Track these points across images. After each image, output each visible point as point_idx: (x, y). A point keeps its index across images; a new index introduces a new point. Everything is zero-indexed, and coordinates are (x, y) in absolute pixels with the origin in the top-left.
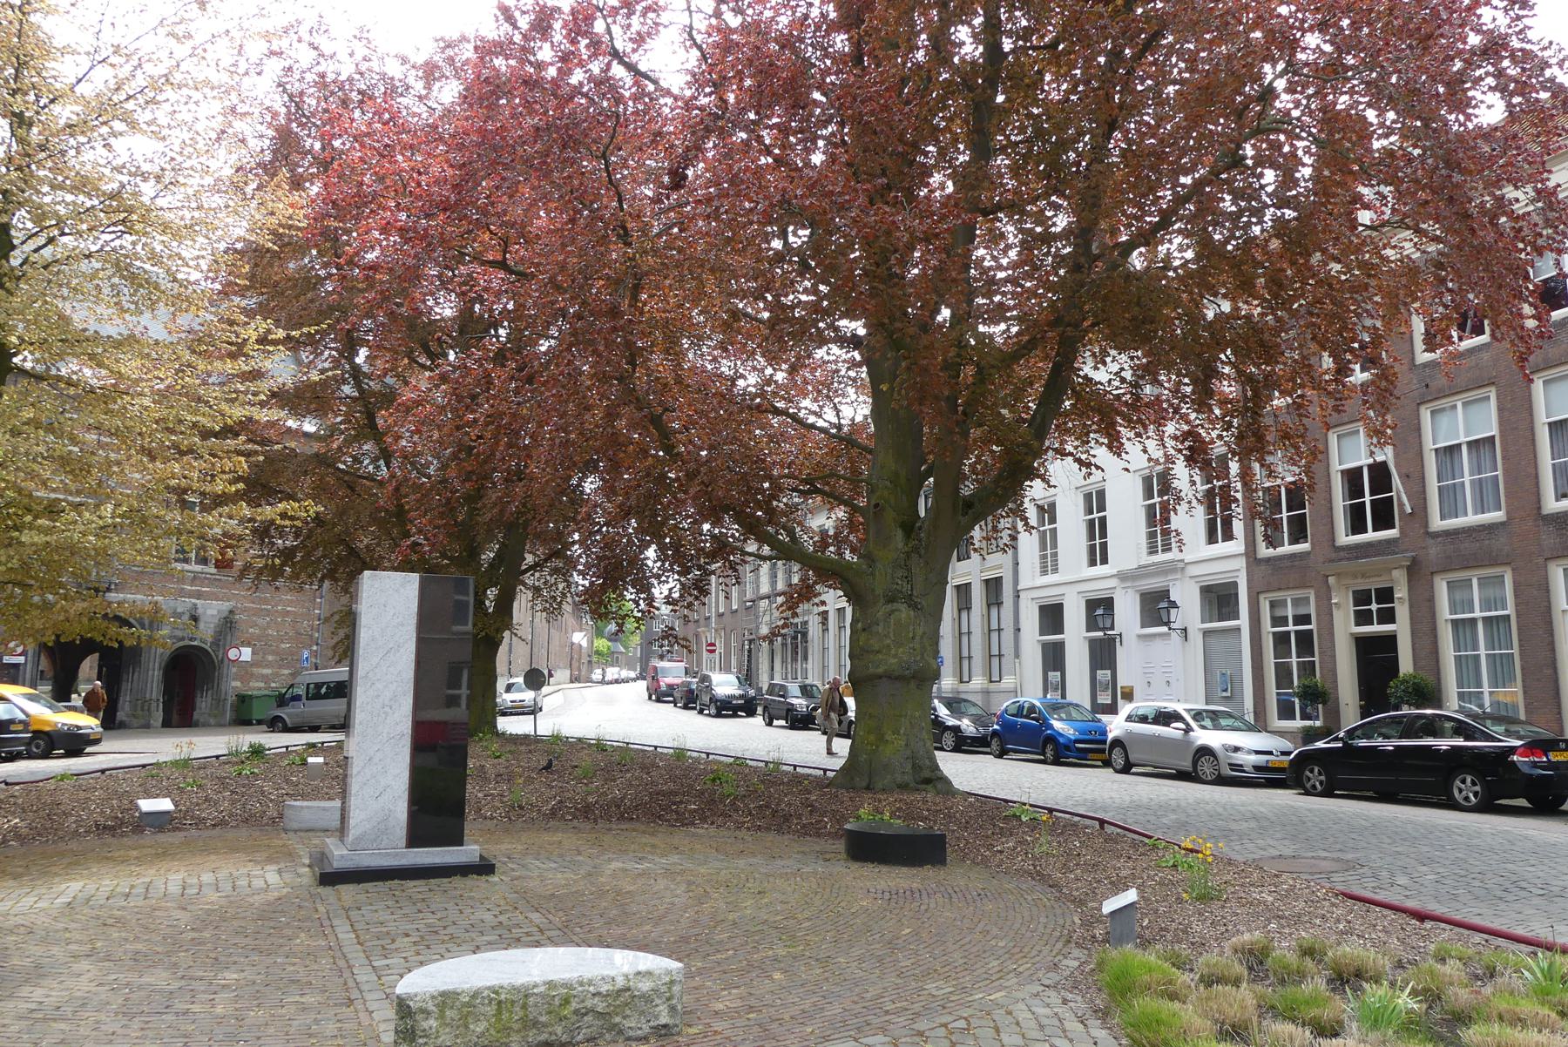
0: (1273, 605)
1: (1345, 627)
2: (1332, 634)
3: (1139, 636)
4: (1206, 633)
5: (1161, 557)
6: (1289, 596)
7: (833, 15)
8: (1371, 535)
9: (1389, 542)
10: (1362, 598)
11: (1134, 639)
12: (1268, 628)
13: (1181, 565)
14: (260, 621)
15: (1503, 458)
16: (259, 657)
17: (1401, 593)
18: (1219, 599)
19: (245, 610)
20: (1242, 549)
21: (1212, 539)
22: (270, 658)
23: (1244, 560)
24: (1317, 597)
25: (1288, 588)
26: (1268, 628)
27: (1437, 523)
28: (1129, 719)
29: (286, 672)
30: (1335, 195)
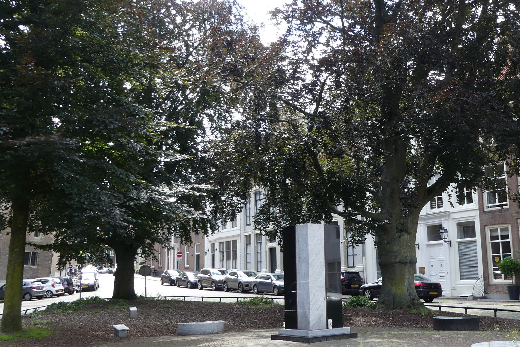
3: (428, 245)
4: (460, 243)
5: (437, 210)
6: (499, 227)
7: (58, 126)
11: (425, 246)
12: (489, 241)
13: (448, 214)
18: (466, 229)
20: (428, 212)
23: (478, 211)
24: (512, 227)
25: (499, 224)
26: (489, 241)
28: (213, 267)
30: (334, 121)
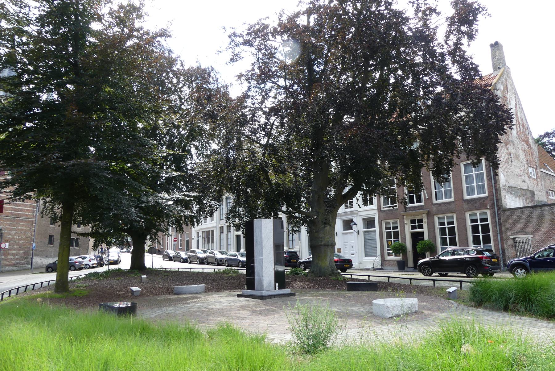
0: (439, 218)
1: (408, 230)
2: (405, 232)
3: (343, 234)
4: (365, 232)
6: (391, 221)
8: (416, 204)
9: (421, 206)
10: (413, 222)
12: (384, 231)
14: (12, 233)
15: (453, 184)
16: (11, 247)
17: (425, 220)
18: (369, 223)
19: (6, 229)
20: (376, 207)
21: (365, 204)
22: (16, 247)
26: (384, 231)
27: (435, 201)
29: (22, 252)
